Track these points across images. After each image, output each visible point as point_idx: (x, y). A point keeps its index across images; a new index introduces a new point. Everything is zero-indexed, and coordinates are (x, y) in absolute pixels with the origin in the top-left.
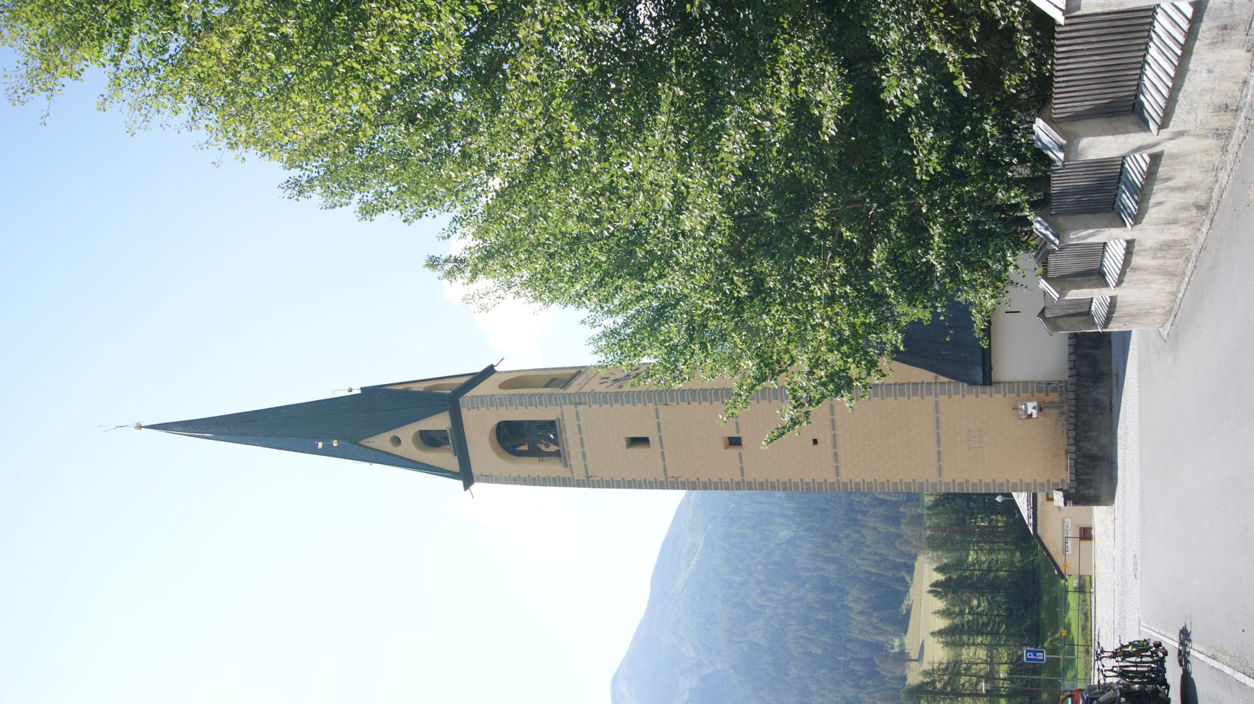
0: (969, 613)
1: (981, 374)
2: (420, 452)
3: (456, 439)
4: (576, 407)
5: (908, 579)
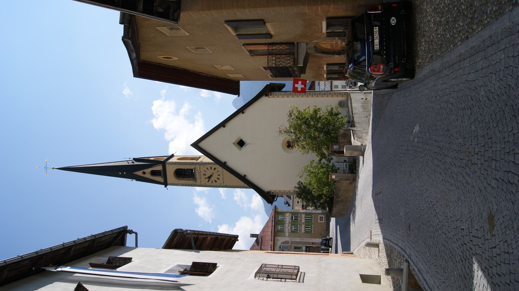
3: (163, 173)
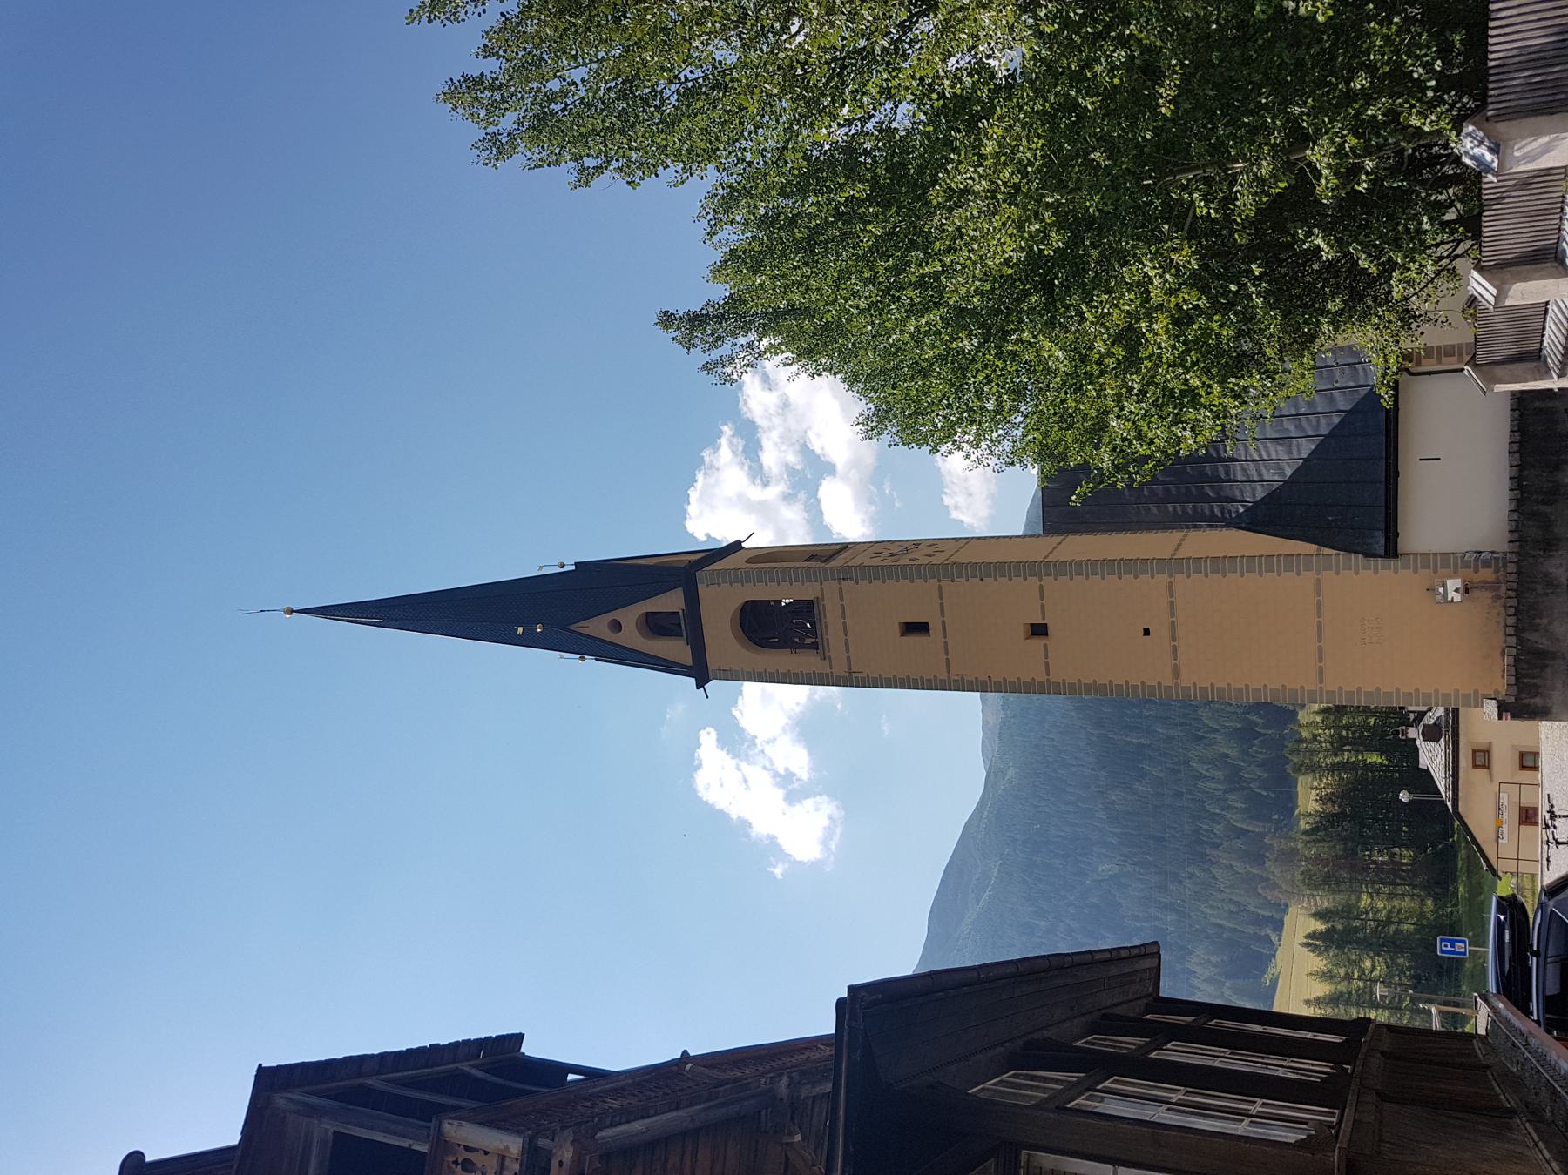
0: (1359, 978)
1: (1382, 541)
2: (644, 640)
3: (687, 626)
4: (840, 584)
5: (1274, 938)
